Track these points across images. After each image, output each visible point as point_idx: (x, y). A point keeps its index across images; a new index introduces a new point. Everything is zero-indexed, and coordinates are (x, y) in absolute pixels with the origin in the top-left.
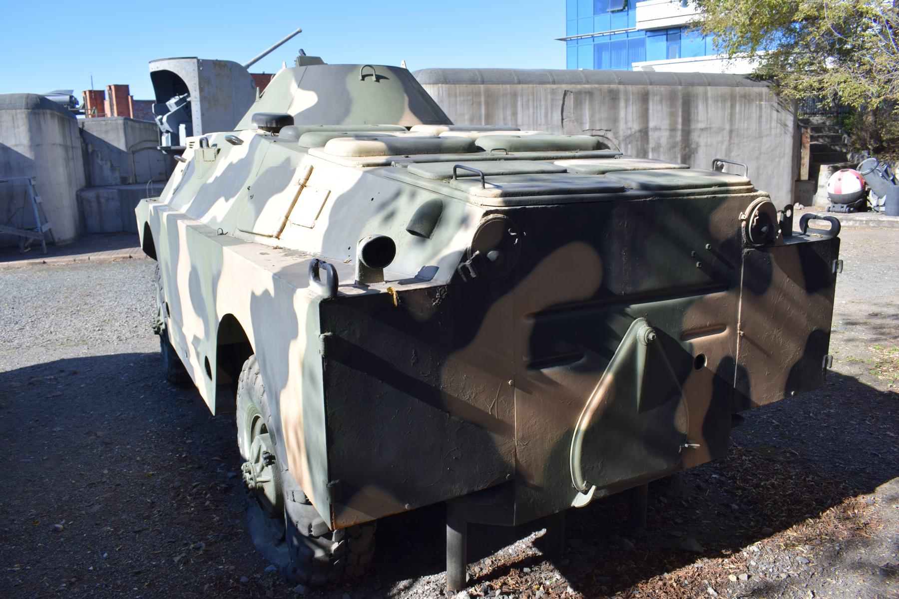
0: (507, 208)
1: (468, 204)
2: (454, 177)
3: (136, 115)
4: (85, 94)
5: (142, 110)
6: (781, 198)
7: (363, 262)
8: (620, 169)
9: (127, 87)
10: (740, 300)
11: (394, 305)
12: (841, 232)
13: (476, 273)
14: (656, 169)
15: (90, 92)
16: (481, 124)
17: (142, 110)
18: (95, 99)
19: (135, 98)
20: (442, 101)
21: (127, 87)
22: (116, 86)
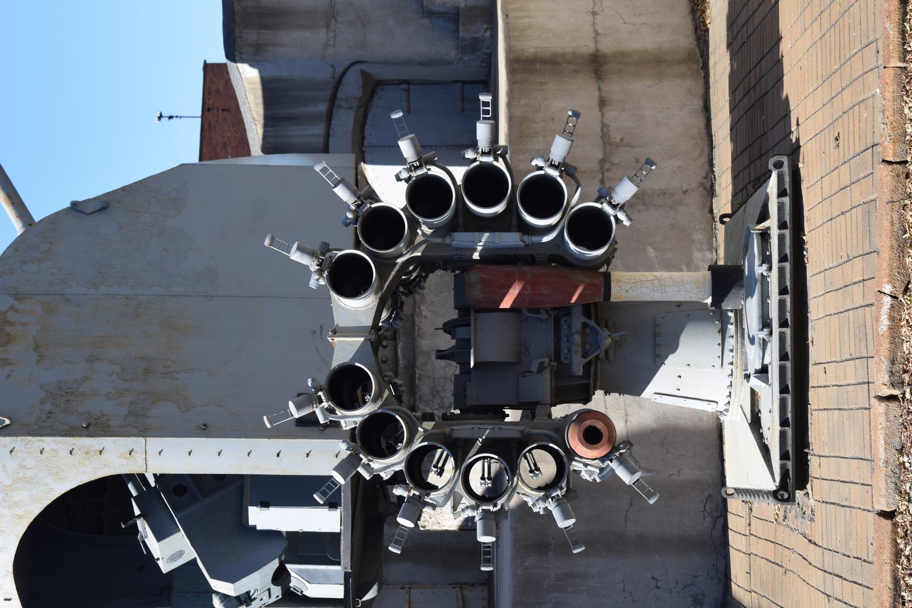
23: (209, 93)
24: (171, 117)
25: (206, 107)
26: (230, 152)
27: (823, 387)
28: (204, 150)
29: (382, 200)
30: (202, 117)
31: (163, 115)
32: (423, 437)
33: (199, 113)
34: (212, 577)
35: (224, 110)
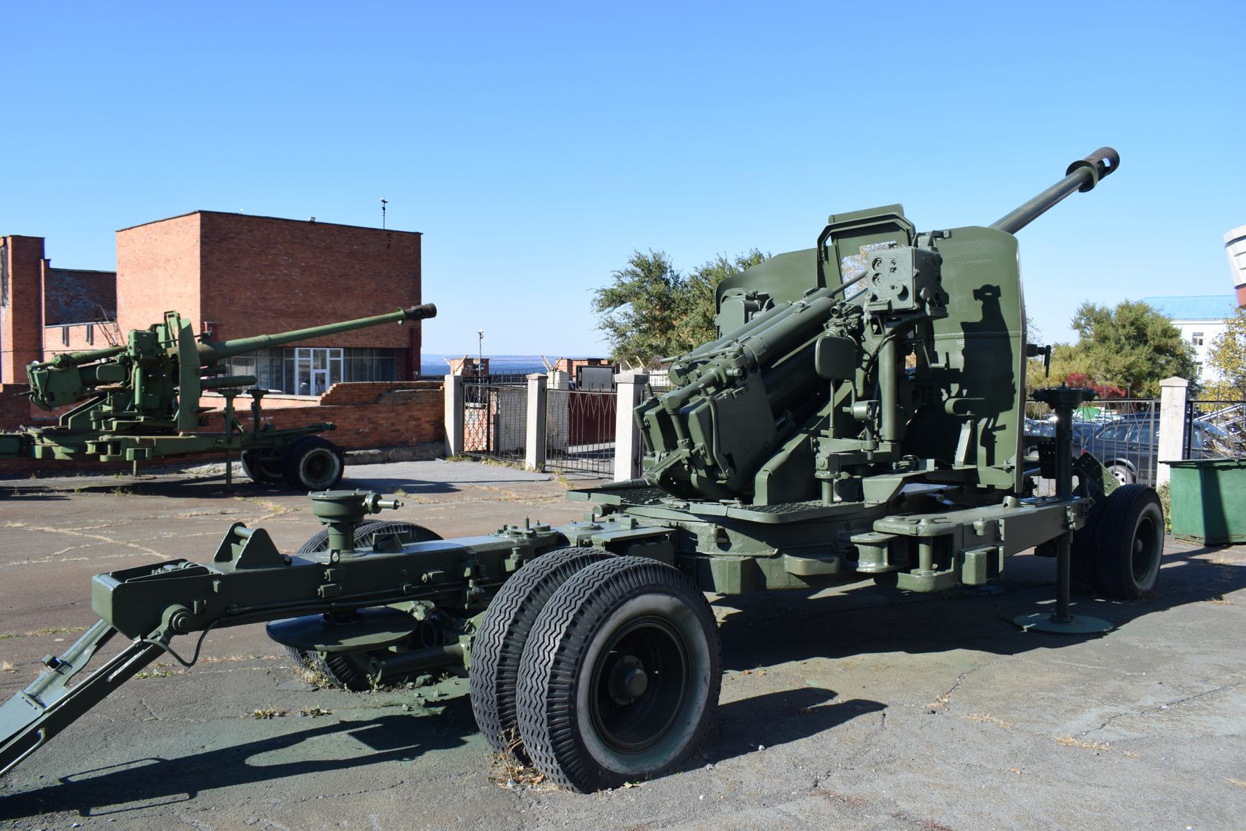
0: (847, 504)
3: (53, 298)
5: (65, 289)
6: (1063, 373)
7: (830, 702)
9: (40, 242)
13: (1005, 539)
16: (314, 351)
17: (65, 289)
19: (52, 265)
20: (1179, 431)
21: (40, 242)
22: (16, 239)
23: (399, 235)
24: (384, 209)
25: (391, 233)
26: (359, 248)
27: (114, 488)
28: (353, 229)
29: (188, 324)
30: (385, 230)
31: (386, 204)
32: (156, 762)
33: (387, 228)
34: (957, 401)
35: (389, 245)
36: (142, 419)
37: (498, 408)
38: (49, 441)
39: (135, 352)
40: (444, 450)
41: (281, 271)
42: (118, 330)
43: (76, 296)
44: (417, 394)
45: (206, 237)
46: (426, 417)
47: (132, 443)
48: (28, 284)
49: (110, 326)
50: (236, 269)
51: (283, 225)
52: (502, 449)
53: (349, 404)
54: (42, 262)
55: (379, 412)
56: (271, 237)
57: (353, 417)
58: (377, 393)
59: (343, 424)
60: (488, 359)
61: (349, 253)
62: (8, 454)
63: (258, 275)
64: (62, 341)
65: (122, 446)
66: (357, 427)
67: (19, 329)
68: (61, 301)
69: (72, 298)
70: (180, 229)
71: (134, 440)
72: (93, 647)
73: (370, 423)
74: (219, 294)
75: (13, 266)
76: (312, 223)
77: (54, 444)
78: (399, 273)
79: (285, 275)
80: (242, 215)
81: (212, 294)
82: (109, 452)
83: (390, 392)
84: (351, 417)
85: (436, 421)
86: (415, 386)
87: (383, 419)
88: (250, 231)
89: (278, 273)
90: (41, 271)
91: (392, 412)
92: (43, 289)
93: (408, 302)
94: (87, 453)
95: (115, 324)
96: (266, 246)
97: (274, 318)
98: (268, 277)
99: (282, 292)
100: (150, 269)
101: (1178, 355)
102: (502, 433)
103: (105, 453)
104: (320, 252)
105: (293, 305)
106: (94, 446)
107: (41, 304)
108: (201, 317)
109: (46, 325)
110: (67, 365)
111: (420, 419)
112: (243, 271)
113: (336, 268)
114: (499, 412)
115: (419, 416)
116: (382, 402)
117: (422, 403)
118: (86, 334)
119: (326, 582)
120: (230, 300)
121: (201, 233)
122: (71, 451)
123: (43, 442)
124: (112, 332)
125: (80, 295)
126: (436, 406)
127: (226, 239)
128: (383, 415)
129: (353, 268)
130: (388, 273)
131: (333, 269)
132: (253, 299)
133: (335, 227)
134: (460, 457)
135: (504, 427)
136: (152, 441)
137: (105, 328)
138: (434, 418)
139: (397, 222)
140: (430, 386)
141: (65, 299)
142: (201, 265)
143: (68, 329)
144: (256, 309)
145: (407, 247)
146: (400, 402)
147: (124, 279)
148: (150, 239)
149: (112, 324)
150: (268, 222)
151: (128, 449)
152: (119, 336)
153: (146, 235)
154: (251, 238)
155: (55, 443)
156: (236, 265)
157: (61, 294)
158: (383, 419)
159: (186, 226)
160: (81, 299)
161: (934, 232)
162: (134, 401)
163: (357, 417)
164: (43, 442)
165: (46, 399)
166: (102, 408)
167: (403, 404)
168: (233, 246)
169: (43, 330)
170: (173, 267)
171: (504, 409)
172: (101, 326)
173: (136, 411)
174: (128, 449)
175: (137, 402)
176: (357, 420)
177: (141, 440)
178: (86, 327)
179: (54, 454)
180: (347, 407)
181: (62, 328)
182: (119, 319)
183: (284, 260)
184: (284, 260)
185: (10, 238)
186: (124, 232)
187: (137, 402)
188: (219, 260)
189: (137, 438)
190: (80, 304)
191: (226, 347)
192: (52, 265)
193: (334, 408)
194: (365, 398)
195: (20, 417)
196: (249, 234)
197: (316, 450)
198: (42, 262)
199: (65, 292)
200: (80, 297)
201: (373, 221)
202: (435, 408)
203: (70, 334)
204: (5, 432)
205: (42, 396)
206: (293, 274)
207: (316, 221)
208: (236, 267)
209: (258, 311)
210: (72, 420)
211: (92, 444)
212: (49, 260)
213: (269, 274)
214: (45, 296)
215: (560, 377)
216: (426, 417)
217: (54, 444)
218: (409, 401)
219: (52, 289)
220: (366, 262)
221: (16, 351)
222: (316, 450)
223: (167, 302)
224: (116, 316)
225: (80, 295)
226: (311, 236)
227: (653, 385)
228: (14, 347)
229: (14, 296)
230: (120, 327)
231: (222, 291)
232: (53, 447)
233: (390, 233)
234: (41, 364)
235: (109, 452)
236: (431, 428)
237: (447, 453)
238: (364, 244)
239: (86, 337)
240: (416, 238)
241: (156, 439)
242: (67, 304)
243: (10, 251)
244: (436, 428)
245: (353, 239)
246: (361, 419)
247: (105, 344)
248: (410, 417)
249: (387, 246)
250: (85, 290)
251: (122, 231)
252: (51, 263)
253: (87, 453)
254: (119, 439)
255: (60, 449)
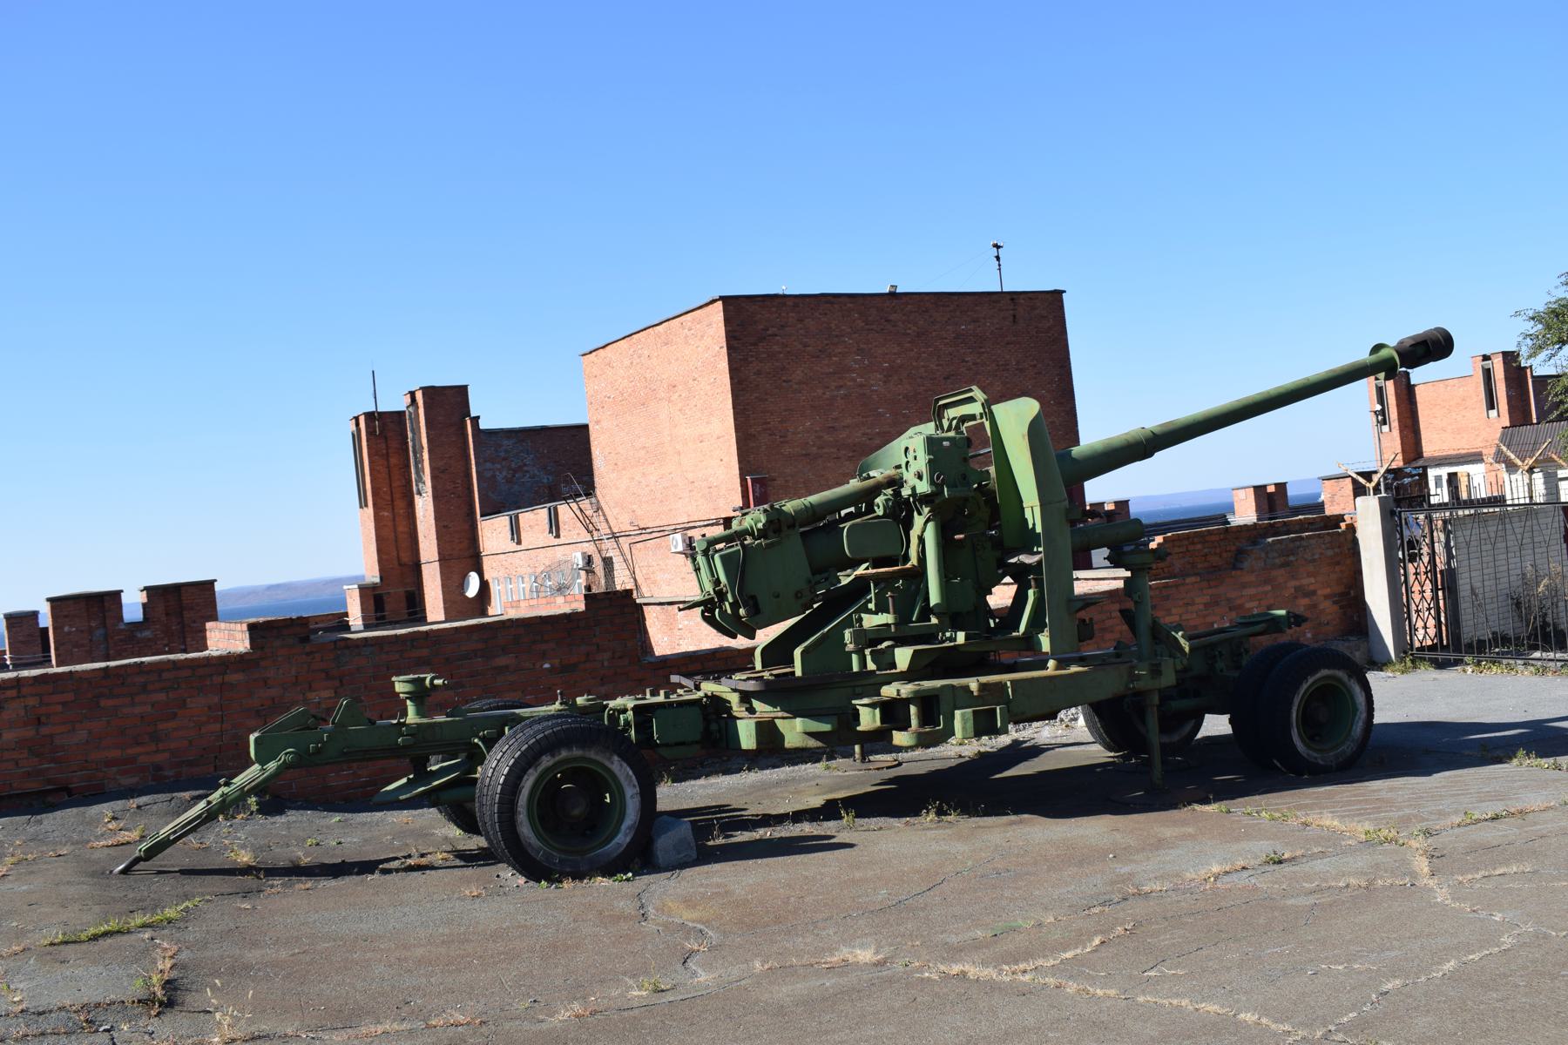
1: (696, 596)
2: (588, 568)
3: (488, 474)
4: (357, 424)
5: (505, 459)
8: (1172, 521)
9: (462, 391)
10: (989, 435)
11: (632, 741)
12: (1375, 698)
14: (780, 819)
15: (370, 416)
17: (505, 459)
18: (383, 436)
19: (483, 425)
21: (462, 391)
22: (426, 390)
24: (998, 258)
25: (1015, 297)
30: (1002, 293)
36: (961, 637)
37: (1450, 556)
38: (768, 708)
39: (932, 483)
40: (1369, 651)
41: (854, 380)
42: (599, 508)
43: (520, 467)
44: (1304, 543)
45: (735, 338)
46: (1323, 585)
47: (962, 698)
48: (450, 457)
49: (585, 503)
50: (784, 384)
51: (849, 305)
52: (1465, 639)
53: (1189, 575)
54: (469, 422)
55: (1244, 586)
56: (833, 326)
57: (1201, 600)
58: (1233, 548)
59: (1184, 617)
60: (1127, 502)
61: (955, 338)
62: (683, 744)
63: (820, 391)
64: (510, 537)
65: (944, 707)
66: (1209, 619)
67: (444, 527)
68: (500, 477)
69: (515, 471)
70: (688, 333)
71: (966, 688)
72: (648, 531)
73: (1230, 609)
74: (766, 429)
75: (427, 433)
76: (893, 295)
77: (780, 714)
78: (1035, 362)
79: (861, 386)
80: (785, 296)
81: (752, 431)
82: (914, 722)
83: (1254, 543)
84: (1198, 600)
85: (1342, 595)
86: (1297, 527)
87: (1251, 598)
88: (801, 321)
89: (849, 383)
90: (468, 435)
91: (1266, 582)
92: (473, 462)
93: (1055, 408)
94: (859, 728)
95: (593, 500)
96: (826, 342)
97: (850, 459)
98: (835, 393)
99: (859, 415)
100: (643, 404)
101: (1503, 462)
102: (1465, 606)
103: (905, 726)
104: (910, 342)
105: (878, 433)
106: (877, 711)
107: (473, 485)
108: (740, 469)
109: (482, 516)
110: (777, 531)
111: (1314, 593)
112: (795, 386)
113: (937, 365)
114: (1454, 564)
115: (1312, 588)
116: (1246, 565)
117: (1314, 560)
118: (547, 521)
119: (404, 736)
120: (781, 437)
121: (727, 332)
122: (826, 727)
123: (751, 710)
124: (589, 512)
125: (525, 465)
126: (1338, 563)
127: (764, 338)
128: (1251, 591)
129: (963, 361)
130: (1018, 363)
131: (933, 366)
132: (816, 431)
133: (914, 296)
134: (1409, 664)
135: (1468, 593)
136: (1001, 686)
137: (581, 510)
138: (1339, 589)
139: (1021, 279)
140: (1322, 524)
141: (504, 473)
142: (732, 384)
143: (517, 517)
144: (823, 448)
145: (1043, 317)
146: (1277, 561)
147: (602, 428)
148: (639, 357)
149: (587, 501)
150: (827, 302)
151: (958, 713)
152: (602, 518)
153: (631, 352)
154: (802, 332)
155: (782, 710)
156: (784, 378)
157: (499, 466)
158: (1251, 598)
159: (698, 326)
160: (527, 472)
161: (961, 416)
162: (927, 599)
163: (1206, 599)
164: (751, 710)
165: (742, 612)
166: (860, 620)
167: (1283, 565)
168: (776, 348)
169: (479, 523)
170: (684, 395)
171: (1463, 557)
172: (574, 506)
173: (934, 620)
174: (958, 713)
175: (934, 598)
176: (1206, 605)
177: (983, 687)
178: (546, 510)
179: (782, 737)
180: (1188, 580)
181: (507, 518)
182: (598, 491)
183: (856, 361)
184: (856, 361)
185: (421, 391)
186: (594, 353)
187: (934, 598)
188: (759, 373)
189: (973, 684)
190: (526, 479)
191: (1074, 460)
192: (483, 425)
193: (1166, 586)
194: (1215, 560)
195: (620, 658)
196: (800, 326)
197: (1319, 675)
198: (469, 422)
199: (504, 463)
200: (525, 468)
201: (985, 282)
202: (1337, 568)
203: (521, 525)
204: (667, 696)
205: (735, 606)
206: (872, 382)
207: (897, 291)
208: (784, 381)
209: (825, 450)
210: (803, 653)
211: (872, 706)
212: (478, 417)
213: (836, 387)
214: (477, 472)
215: (1545, 483)
216: (1323, 585)
217: (780, 714)
218: (1292, 558)
219: (485, 461)
220: (983, 350)
221: (443, 559)
222: (1319, 675)
223: (679, 453)
224: (593, 488)
225: (525, 465)
226: (893, 317)
227: (1545, 498)
228: (439, 553)
229: (434, 478)
230: (603, 504)
231: (769, 423)
232: (778, 722)
233: (1014, 296)
234: (728, 532)
235: (914, 722)
236: (1336, 607)
237: (1377, 658)
238: (975, 321)
239: (547, 527)
240: (1053, 301)
241: (1012, 682)
242: (509, 481)
243: (421, 411)
244: (1341, 607)
245: (958, 313)
246: (1214, 603)
247: (578, 534)
248: (1297, 589)
249: (1011, 319)
250: (532, 456)
251: (591, 352)
252: (480, 421)
253: (859, 728)
254: (934, 689)
255: (799, 723)
